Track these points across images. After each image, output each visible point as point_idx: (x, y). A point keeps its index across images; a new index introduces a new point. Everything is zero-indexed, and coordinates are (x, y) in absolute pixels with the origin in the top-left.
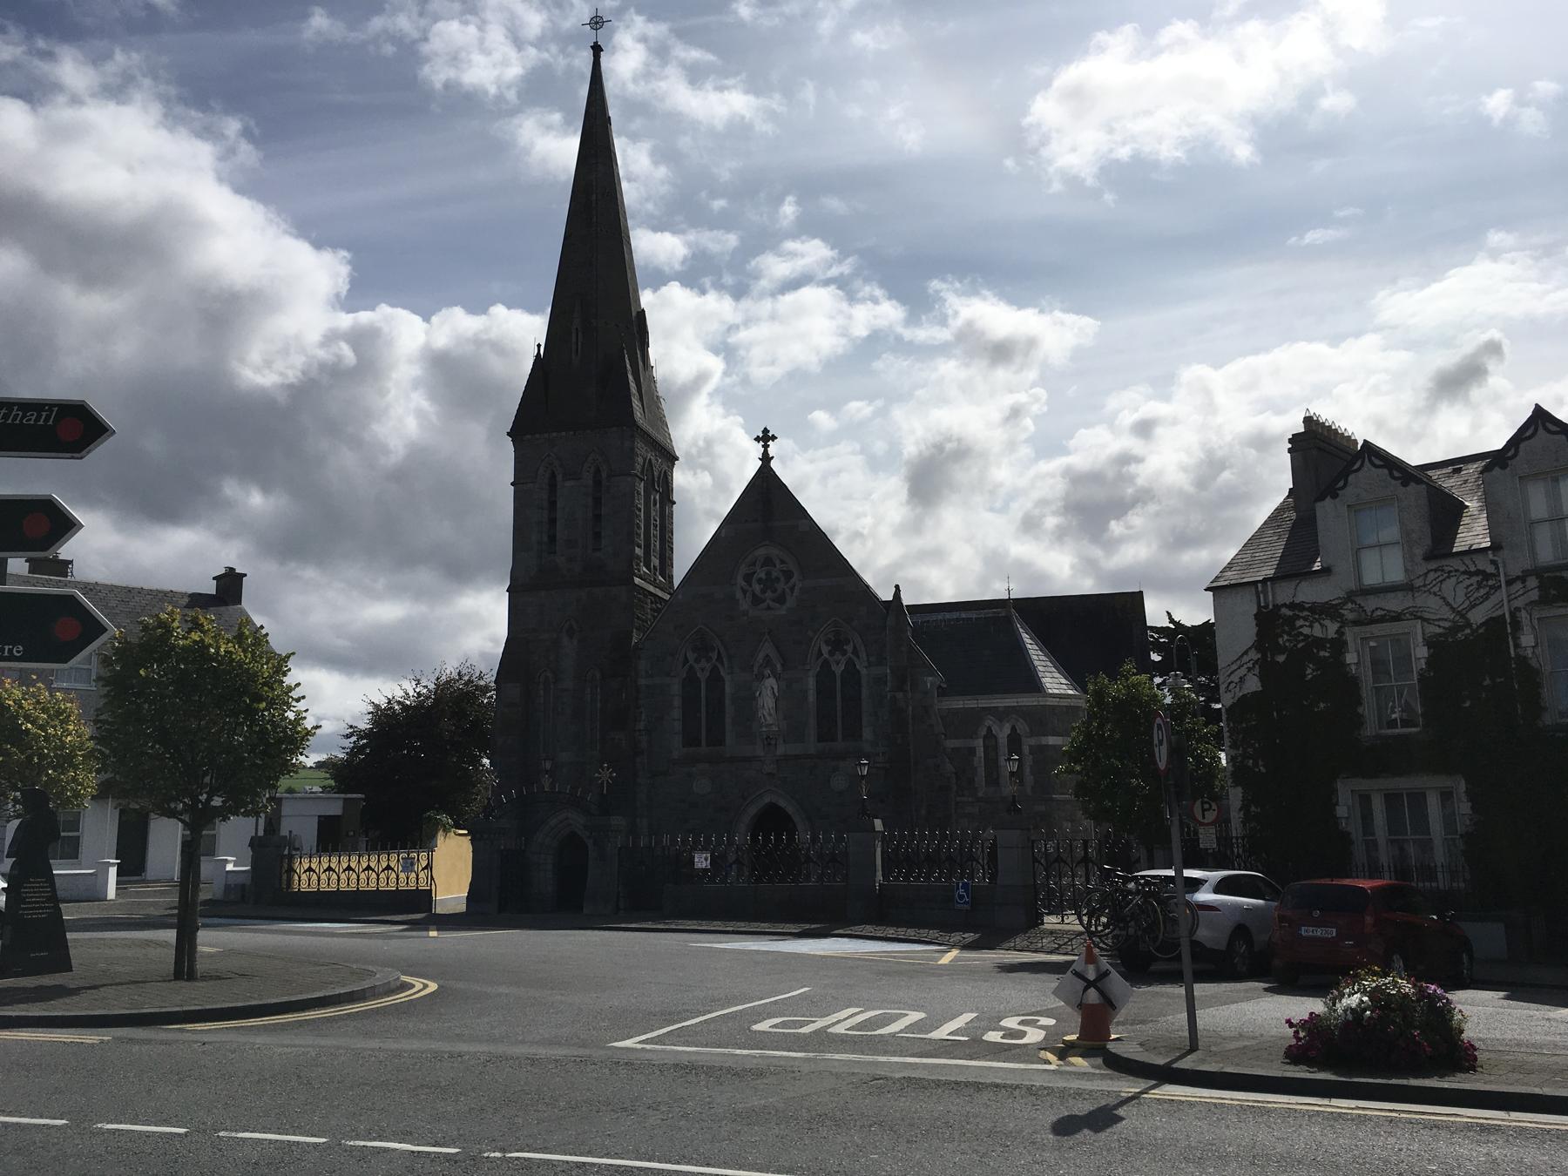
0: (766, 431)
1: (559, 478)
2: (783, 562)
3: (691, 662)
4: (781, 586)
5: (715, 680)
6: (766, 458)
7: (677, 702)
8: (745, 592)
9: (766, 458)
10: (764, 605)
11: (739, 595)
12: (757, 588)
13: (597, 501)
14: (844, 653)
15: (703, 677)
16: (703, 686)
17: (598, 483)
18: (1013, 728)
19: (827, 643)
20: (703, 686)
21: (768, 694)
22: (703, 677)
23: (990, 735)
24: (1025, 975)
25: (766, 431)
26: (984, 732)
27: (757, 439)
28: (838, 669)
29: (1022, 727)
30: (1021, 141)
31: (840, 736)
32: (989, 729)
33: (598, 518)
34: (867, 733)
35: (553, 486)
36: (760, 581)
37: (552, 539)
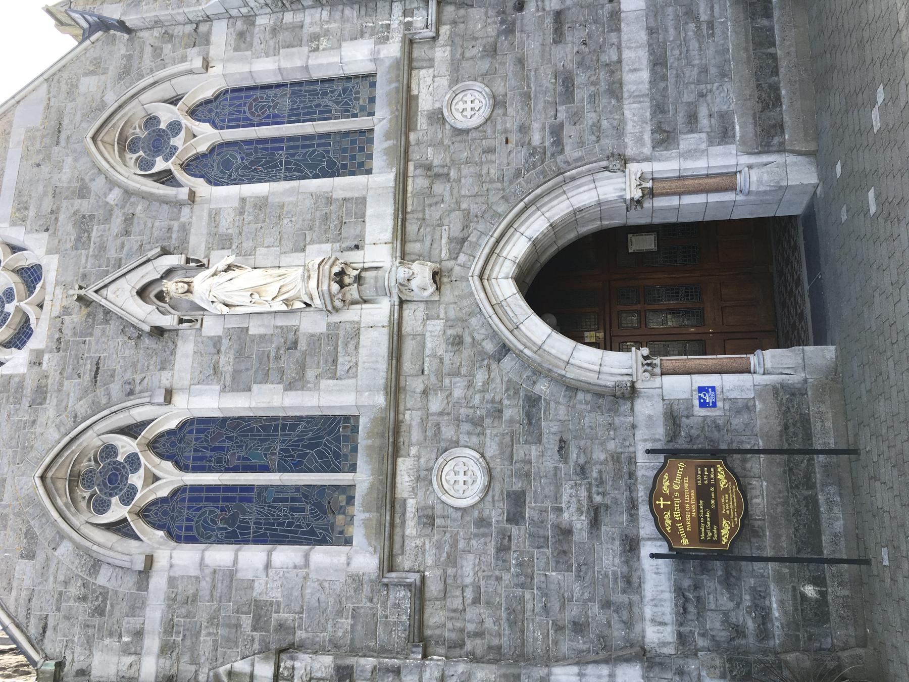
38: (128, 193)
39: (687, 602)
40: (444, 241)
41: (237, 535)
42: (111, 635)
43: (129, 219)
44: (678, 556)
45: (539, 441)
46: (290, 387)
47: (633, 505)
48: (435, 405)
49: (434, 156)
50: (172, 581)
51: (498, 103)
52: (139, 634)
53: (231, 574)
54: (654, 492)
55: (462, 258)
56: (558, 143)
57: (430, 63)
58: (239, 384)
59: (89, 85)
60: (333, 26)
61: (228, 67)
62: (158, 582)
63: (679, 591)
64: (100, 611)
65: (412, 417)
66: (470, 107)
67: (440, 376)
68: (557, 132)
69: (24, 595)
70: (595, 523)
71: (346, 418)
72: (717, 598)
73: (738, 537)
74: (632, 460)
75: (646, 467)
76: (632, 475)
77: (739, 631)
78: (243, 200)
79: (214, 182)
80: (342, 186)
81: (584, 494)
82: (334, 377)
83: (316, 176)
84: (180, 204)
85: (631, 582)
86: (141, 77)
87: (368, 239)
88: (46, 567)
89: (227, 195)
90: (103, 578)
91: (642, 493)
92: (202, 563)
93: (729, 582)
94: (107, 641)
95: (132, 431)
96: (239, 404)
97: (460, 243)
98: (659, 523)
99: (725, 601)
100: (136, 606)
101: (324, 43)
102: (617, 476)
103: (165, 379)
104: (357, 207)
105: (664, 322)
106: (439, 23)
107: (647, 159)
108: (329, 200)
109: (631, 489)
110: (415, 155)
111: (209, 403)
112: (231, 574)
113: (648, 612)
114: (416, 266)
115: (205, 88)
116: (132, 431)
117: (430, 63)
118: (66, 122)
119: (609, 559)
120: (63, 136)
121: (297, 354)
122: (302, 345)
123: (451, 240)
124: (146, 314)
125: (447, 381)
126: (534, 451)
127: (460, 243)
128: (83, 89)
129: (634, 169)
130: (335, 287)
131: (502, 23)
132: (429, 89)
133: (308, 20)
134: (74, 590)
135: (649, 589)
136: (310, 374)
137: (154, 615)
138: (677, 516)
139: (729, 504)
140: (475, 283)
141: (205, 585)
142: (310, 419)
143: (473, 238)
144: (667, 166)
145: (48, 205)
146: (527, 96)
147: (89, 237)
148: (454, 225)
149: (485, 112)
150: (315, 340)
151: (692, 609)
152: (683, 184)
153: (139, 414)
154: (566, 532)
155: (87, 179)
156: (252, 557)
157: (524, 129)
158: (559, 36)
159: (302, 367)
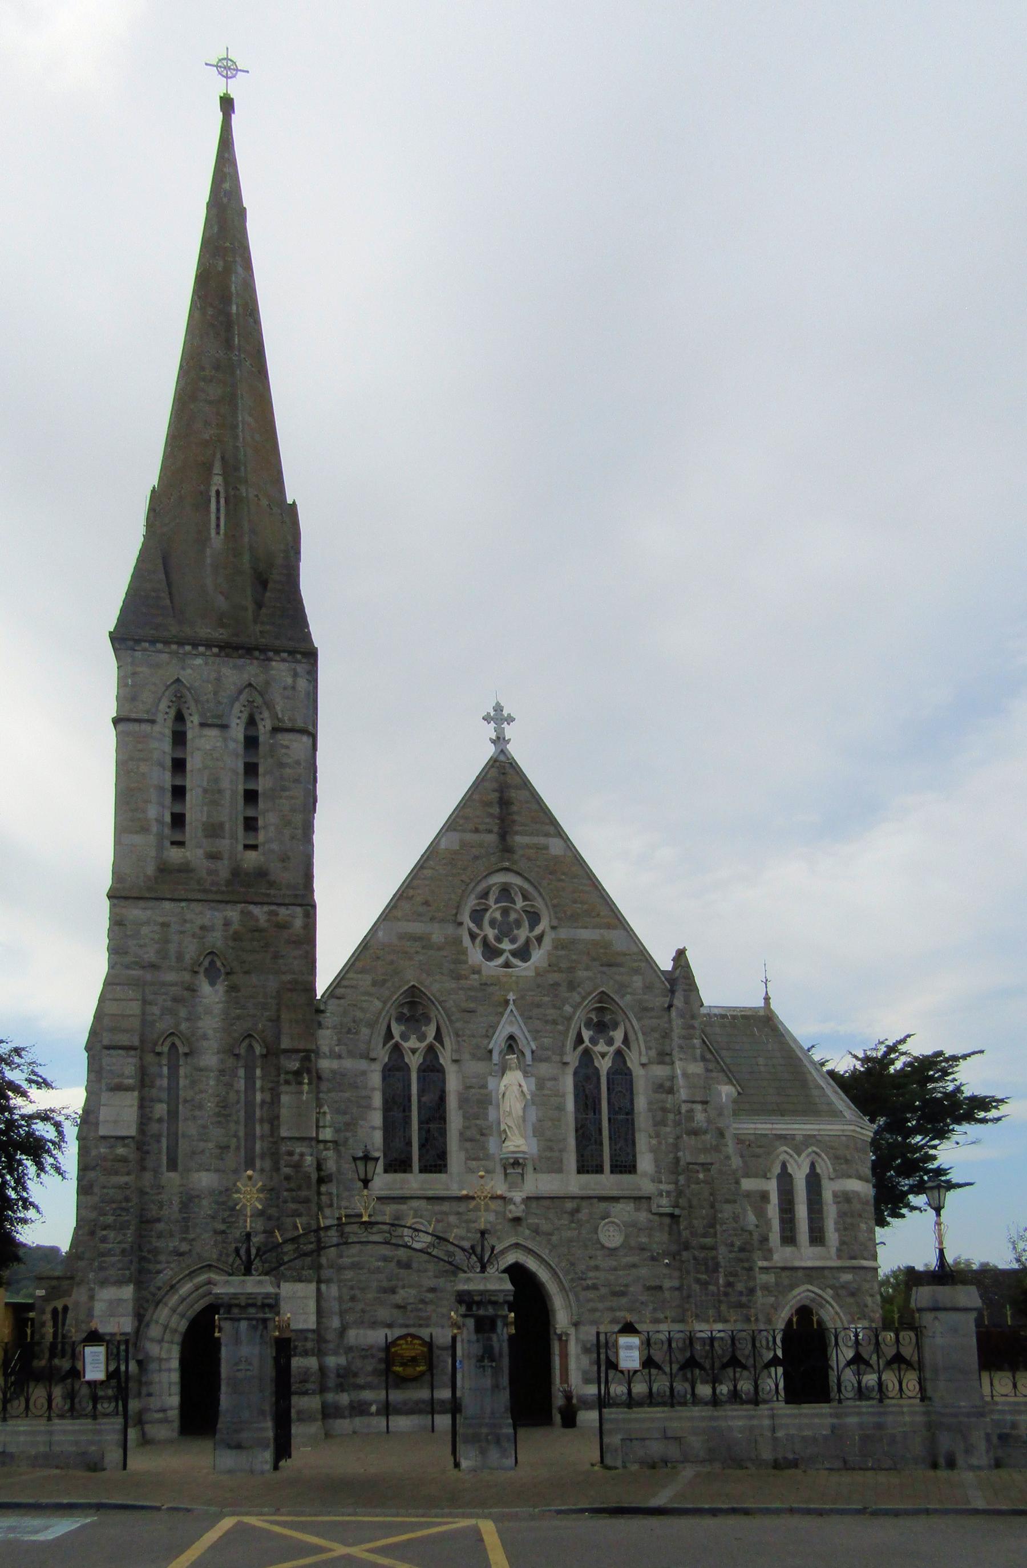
0: (498, 708)
1: (193, 720)
2: (525, 898)
3: (397, 1038)
4: (523, 934)
5: (432, 1069)
6: (499, 740)
7: (377, 1100)
8: (473, 936)
9: (499, 740)
10: (500, 961)
11: (467, 941)
12: (491, 933)
13: (251, 770)
14: (610, 1042)
15: (414, 1062)
16: (414, 1076)
17: (251, 742)
18: (813, 1166)
19: (589, 1024)
20: (414, 1076)
21: (512, 1088)
22: (414, 1062)
23: (785, 1178)
24: (574, 1516)
25: (498, 708)
26: (777, 1170)
27: (487, 718)
28: (604, 1065)
29: (825, 1167)
30: (335, 1329)
31: (607, 1167)
32: (784, 1166)
33: (251, 797)
34: (645, 1163)
35: (179, 738)
36: (493, 923)
37: (178, 821)
38: (569, 1019)
39: (365, 1352)
40: (536, 1221)
41: (388, 1107)
42: (339, 1040)
43: (555, 1022)
44: (388, 1346)
45: (436, 1277)
46: (461, 1134)
47: (407, 1326)
48: (452, 1219)
49: (583, 1215)
50: (364, 1073)
51: (612, 1252)
52: (339, 1057)
53: (369, 1107)
54: (414, 1337)
55: (527, 1232)
56: (587, 1288)
57: (637, 1210)
58: (463, 1101)
59: (638, 982)
60: (663, 1147)
61: (644, 1078)
62: (363, 1065)
63: (371, 1347)
64: (349, 1031)
65: (446, 1207)
66: (611, 1237)
67: (467, 1222)
68: (595, 1287)
69: (365, 1005)
70: (398, 1307)
71: (445, 1166)
72: (370, 1365)
73: (397, 1374)
74: (427, 1326)
75: (424, 1333)
76: (420, 1326)
77: (356, 1375)
78: (563, 1096)
79: (575, 1073)
80: (571, 1160)
81: (411, 1301)
82: (467, 1159)
83: (577, 1139)
84: (562, 1054)
85: (374, 1325)
86: (639, 1019)
87: (540, 1176)
88: (370, 994)
89: (568, 1084)
90: (365, 1031)
91: (412, 1330)
92: (374, 1089)
93: (375, 1372)
94: (335, 1038)
95: (438, 1037)
96: (452, 1102)
97: (536, 1231)
98: (400, 1338)
99: (370, 1368)
100: (351, 1054)
101: (654, 1142)
102: (420, 1318)
103: (466, 1056)
104: (555, 1167)
105: (486, 1310)
106: (661, 1215)
107: (577, 1339)
108: (561, 1151)
109: (414, 1326)
110: (584, 1203)
111: (453, 1084)
112: (369, 1107)
113: (362, 1331)
114: (523, 1207)
115: (633, 1061)
116: (438, 1037)
117: (637, 1210)
118: (614, 969)
119: (383, 1313)
120: (604, 969)
121: (478, 1137)
122: (483, 1138)
123: (537, 1225)
124: (498, 1042)
125: (464, 1225)
126: (431, 1274)
127: (536, 1231)
128: (635, 978)
129: (572, 1331)
130: (512, 1161)
131: (658, 1253)
132: (623, 1211)
133: (668, 1129)
134: (359, 1015)
135: (370, 1333)
136: (468, 1145)
137: (348, 1064)
138: (404, 1346)
139: (410, 1371)
140: (513, 1240)
141: (364, 1093)
142: (445, 1143)
143: (538, 1238)
144: (573, 1348)
145: (564, 965)
146: (615, 1269)
147: (544, 996)
148: (546, 1227)
149: (607, 1244)
150: (484, 1148)
151: (363, 1353)
152: (564, 1356)
153: (447, 1040)
154: (393, 1291)
155: (579, 989)
156: (377, 1118)
157: (597, 1268)
158: (649, 1288)
159: (471, 1140)
